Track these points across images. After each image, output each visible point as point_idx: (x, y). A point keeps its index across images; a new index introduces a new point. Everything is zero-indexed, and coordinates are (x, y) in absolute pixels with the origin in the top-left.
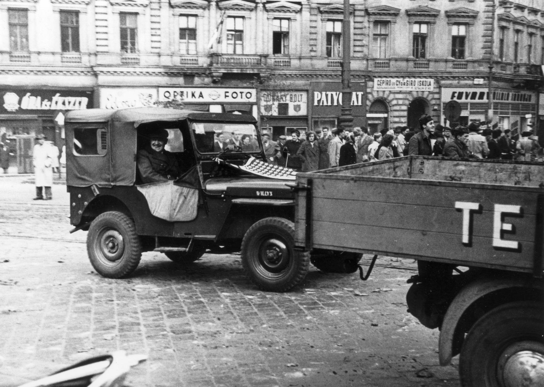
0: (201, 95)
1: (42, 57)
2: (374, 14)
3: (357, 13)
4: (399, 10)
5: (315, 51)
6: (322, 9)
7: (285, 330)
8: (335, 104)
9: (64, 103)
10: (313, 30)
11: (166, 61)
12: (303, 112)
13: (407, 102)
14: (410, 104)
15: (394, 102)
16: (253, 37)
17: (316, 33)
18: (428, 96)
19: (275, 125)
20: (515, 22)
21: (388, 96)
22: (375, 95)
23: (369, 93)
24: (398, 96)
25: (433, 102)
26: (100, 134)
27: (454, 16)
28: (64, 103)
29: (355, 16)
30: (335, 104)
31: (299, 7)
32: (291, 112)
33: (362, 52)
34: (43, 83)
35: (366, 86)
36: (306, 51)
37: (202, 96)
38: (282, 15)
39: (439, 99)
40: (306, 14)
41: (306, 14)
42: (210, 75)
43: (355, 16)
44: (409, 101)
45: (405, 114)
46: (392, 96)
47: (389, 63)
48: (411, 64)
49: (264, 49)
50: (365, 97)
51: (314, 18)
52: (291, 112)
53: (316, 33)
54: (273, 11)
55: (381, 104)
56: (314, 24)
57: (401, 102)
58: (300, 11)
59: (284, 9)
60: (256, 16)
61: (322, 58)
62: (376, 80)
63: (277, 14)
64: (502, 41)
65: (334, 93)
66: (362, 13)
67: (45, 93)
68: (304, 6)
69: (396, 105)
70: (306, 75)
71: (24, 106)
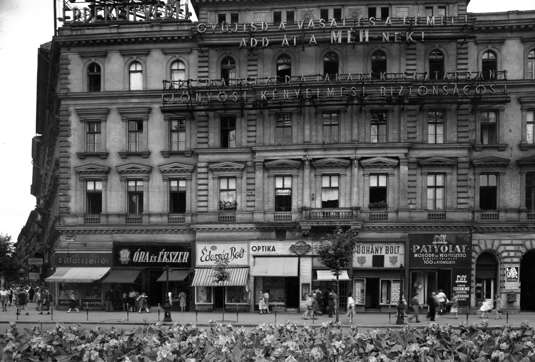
2: (480, 166)
3: (460, 165)
4: (509, 160)
5: (414, 204)
7: (471, 139)
9: (168, 257)
10: (412, 184)
11: (259, 217)
13: (519, 254)
14: (523, 256)
15: (505, 254)
16: (348, 192)
17: (415, 187)
19: (368, 277)
21: (498, 248)
22: (483, 247)
23: (476, 245)
24: (508, 248)
28: (168, 257)
29: (458, 169)
31: (396, 162)
32: (387, 264)
33: (467, 204)
35: (471, 239)
36: (403, 203)
37: (275, 250)
38: (378, 170)
40: (404, 169)
41: (404, 169)
42: (300, 230)
43: (458, 169)
44: (522, 252)
46: (502, 248)
47: (498, 215)
48: (524, 215)
49: (359, 203)
52: (387, 264)
53: (415, 187)
56: (413, 178)
57: (512, 254)
58: (398, 166)
59: (380, 164)
60: (351, 173)
63: (373, 170)
66: (467, 165)
67: (154, 248)
68: (401, 161)
69: (506, 257)
70: (403, 227)
71: (135, 259)
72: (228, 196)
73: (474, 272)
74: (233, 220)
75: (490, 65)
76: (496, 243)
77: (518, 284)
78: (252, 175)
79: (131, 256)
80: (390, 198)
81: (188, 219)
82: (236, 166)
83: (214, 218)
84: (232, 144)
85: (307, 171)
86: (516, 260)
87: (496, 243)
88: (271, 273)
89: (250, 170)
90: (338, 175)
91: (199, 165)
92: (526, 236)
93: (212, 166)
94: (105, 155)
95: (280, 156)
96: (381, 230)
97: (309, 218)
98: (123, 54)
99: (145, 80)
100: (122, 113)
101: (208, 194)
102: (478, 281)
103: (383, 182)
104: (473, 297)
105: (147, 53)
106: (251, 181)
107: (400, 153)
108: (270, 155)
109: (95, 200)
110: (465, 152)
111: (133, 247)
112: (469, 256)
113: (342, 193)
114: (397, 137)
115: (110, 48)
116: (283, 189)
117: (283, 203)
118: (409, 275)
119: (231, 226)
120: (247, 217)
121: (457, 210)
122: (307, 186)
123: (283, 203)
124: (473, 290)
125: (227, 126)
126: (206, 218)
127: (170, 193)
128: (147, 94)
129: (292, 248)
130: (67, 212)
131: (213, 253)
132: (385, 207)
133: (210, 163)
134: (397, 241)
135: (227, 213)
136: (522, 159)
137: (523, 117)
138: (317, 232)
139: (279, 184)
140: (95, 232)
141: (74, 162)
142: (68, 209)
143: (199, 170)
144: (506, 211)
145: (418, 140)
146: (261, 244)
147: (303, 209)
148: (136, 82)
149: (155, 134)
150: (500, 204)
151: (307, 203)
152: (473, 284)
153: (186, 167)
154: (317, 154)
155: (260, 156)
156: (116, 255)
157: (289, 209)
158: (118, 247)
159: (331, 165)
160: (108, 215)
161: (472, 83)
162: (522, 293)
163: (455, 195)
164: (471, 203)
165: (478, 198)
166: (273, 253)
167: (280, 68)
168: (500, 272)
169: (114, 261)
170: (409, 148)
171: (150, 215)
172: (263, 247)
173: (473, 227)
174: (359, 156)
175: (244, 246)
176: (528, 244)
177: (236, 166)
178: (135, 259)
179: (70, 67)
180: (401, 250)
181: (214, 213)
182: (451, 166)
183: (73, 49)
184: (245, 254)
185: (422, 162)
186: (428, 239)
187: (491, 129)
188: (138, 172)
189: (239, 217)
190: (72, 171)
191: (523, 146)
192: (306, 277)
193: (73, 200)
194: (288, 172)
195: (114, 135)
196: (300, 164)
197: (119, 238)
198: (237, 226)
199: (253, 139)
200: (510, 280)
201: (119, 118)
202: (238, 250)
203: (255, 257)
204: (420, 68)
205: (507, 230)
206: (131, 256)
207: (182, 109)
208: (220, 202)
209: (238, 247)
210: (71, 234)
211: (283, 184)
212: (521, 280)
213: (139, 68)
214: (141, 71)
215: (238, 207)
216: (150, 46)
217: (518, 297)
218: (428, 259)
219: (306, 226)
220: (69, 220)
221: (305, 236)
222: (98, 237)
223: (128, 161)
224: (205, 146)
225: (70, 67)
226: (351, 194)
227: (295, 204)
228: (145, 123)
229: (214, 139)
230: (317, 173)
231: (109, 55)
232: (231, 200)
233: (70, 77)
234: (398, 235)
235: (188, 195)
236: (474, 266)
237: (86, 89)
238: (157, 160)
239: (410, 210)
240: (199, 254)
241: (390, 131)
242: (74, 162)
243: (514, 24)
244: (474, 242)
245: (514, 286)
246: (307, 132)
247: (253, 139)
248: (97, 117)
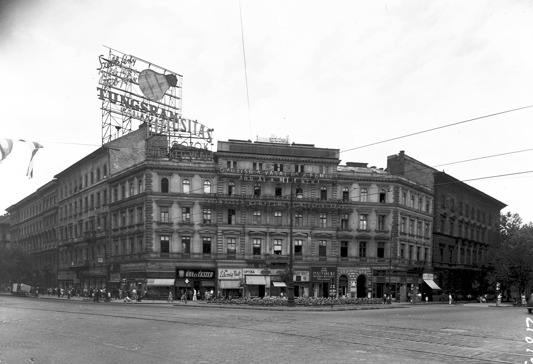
3: (333, 238)
9: (203, 275)
10: (313, 245)
11: (246, 257)
12: (308, 280)
15: (351, 276)
20: (409, 242)
25: (369, 276)
27: (403, 241)
28: (203, 275)
32: (302, 280)
34: (101, 308)
36: (309, 253)
38: (298, 238)
42: (265, 264)
46: (349, 274)
48: (358, 260)
51: (313, 240)
52: (302, 280)
56: (313, 242)
57: (353, 276)
58: (307, 237)
61: (317, 257)
64: (402, 251)
72: (232, 246)
73: (338, 284)
74: (234, 258)
75: (346, 194)
76: (347, 271)
77: (356, 289)
78: (243, 238)
79: (185, 274)
80: (303, 250)
81: (213, 256)
82: (236, 233)
83: (225, 257)
84: (233, 222)
85: (268, 238)
86: (355, 279)
87: (347, 271)
88: (254, 283)
89: (242, 235)
90: (281, 240)
91: (219, 231)
92: (359, 269)
93: (225, 232)
94: (171, 224)
95: (256, 230)
96: (300, 265)
97: (270, 259)
98: (180, 175)
99: (191, 188)
100: (179, 203)
101: (223, 245)
102: (340, 287)
103: (300, 243)
104: (338, 294)
105: (192, 176)
106: (243, 240)
107: (308, 231)
108: (252, 229)
109: (165, 246)
110: (335, 232)
111: (185, 270)
112: (336, 277)
113: (283, 248)
114: (306, 224)
115: (173, 171)
116: (257, 244)
117: (257, 251)
118: (311, 285)
119: (234, 261)
120: (241, 257)
121: (331, 257)
122: (268, 244)
123: (257, 251)
124: (338, 291)
125: (232, 212)
126: (222, 257)
127: (203, 245)
128: (192, 195)
129: (262, 272)
130: (152, 251)
131: (226, 273)
132: (301, 254)
133: (223, 230)
134: (306, 270)
135: (231, 255)
136: (358, 236)
137: (359, 218)
138: (274, 265)
139: (255, 242)
140: (166, 262)
141: (154, 226)
142: (152, 250)
143: (218, 234)
144: (351, 257)
145: (315, 226)
146: (248, 270)
147: (266, 255)
148: (186, 189)
149: (196, 216)
150: (349, 255)
151: (268, 251)
152: (338, 289)
153: (212, 232)
154: (273, 230)
155: (248, 229)
156: (178, 274)
157: (259, 254)
158: (178, 270)
159: (279, 235)
160: (173, 253)
161: (339, 203)
162: (358, 293)
163: (331, 250)
164: (337, 253)
165: (340, 252)
166: (253, 274)
167: (256, 189)
168: (349, 284)
169: (177, 277)
170: (312, 229)
171: (194, 254)
173: (338, 264)
175: (240, 270)
176: (360, 272)
178: (187, 275)
179: (152, 178)
180: (308, 274)
181: (225, 254)
182: (329, 238)
183: (154, 170)
184: (241, 274)
185: (317, 235)
186: (318, 269)
187: (346, 221)
188: (189, 233)
189: (237, 256)
190: (153, 231)
191: (358, 230)
192: (268, 285)
193: (154, 245)
194: (259, 237)
195: (176, 214)
196: (265, 234)
197: (178, 264)
198: (237, 261)
199: (243, 221)
200: (353, 287)
201: (178, 206)
202: (238, 272)
203: (245, 275)
204: (317, 195)
205: (351, 266)
206: (185, 274)
207: (210, 204)
208: (228, 249)
209: (238, 271)
210: (153, 262)
211: (256, 243)
212: (357, 287)
213: (188, 182)
214: (189, 184)
215: (237, 252)
216: (194, 173)
217: (356, 294)
218: (319, 278)
219: (268, 262)
220: (152, 255)
221: (267, 266)
222: (167, 264)
223: (182, 227)
224: (221, 223)
225: (152, 178)
226: (287, 248)
227: (262, 251)
228: (191, 209)
229: (225, 220)
232: (233, 248)
233: (152, 184)
234: (307, 267)
235: (212, 245)
236: (338, 281)
237: (160, 191)
238: (197, 228)
239: (312, 256)
240: (219, 274)
241: (304, 221)
243: (356, 178)
244: (338, 271)
245: (354, 290)
246: (268, 220)
247: (243, 221)
248: (166, 205)
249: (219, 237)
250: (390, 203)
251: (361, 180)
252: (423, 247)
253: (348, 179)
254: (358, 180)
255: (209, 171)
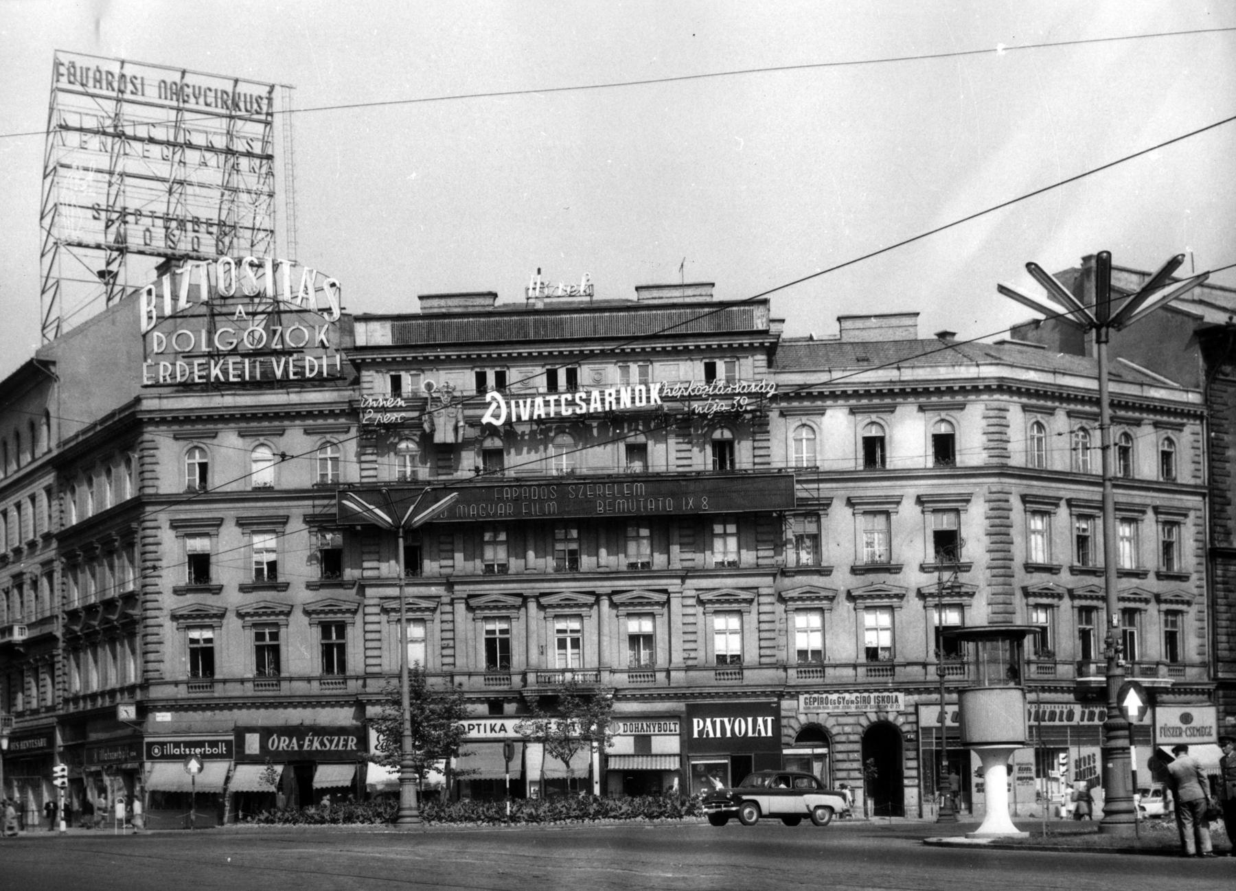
0: (503, 728)
1: (295, 684)
6: (702, 597)
8: (729, 735)
9: (322, 744)
13: (860, 729)
18: (896, 718)
24: (842, 720)
26: (877, 818)
30: (729, 735)
31: (664, 597)
39: (917, 723)
45: (858, 747)
50: (777, 726)
54: (623, 604)
55: (814, 733)
57: (848, 729)
62: (802, 698)
65: (726, 720)
82: (424, 604)
91: (367, 602)
109: (203, 657)
121: (761, 666)
172: (479, 725)
174: (537, 592)
177: (424, 604)
230: (620, 613)
231: (220, 435)
237: (930, 462)
238: (301, 595)
242: (169, 602)
249: (369, 619)
250: (658, 474)
251: (856, 394)
252: (1152, 608)
253: (950, 391)
254: (845, 395)
255: (332, 414)
